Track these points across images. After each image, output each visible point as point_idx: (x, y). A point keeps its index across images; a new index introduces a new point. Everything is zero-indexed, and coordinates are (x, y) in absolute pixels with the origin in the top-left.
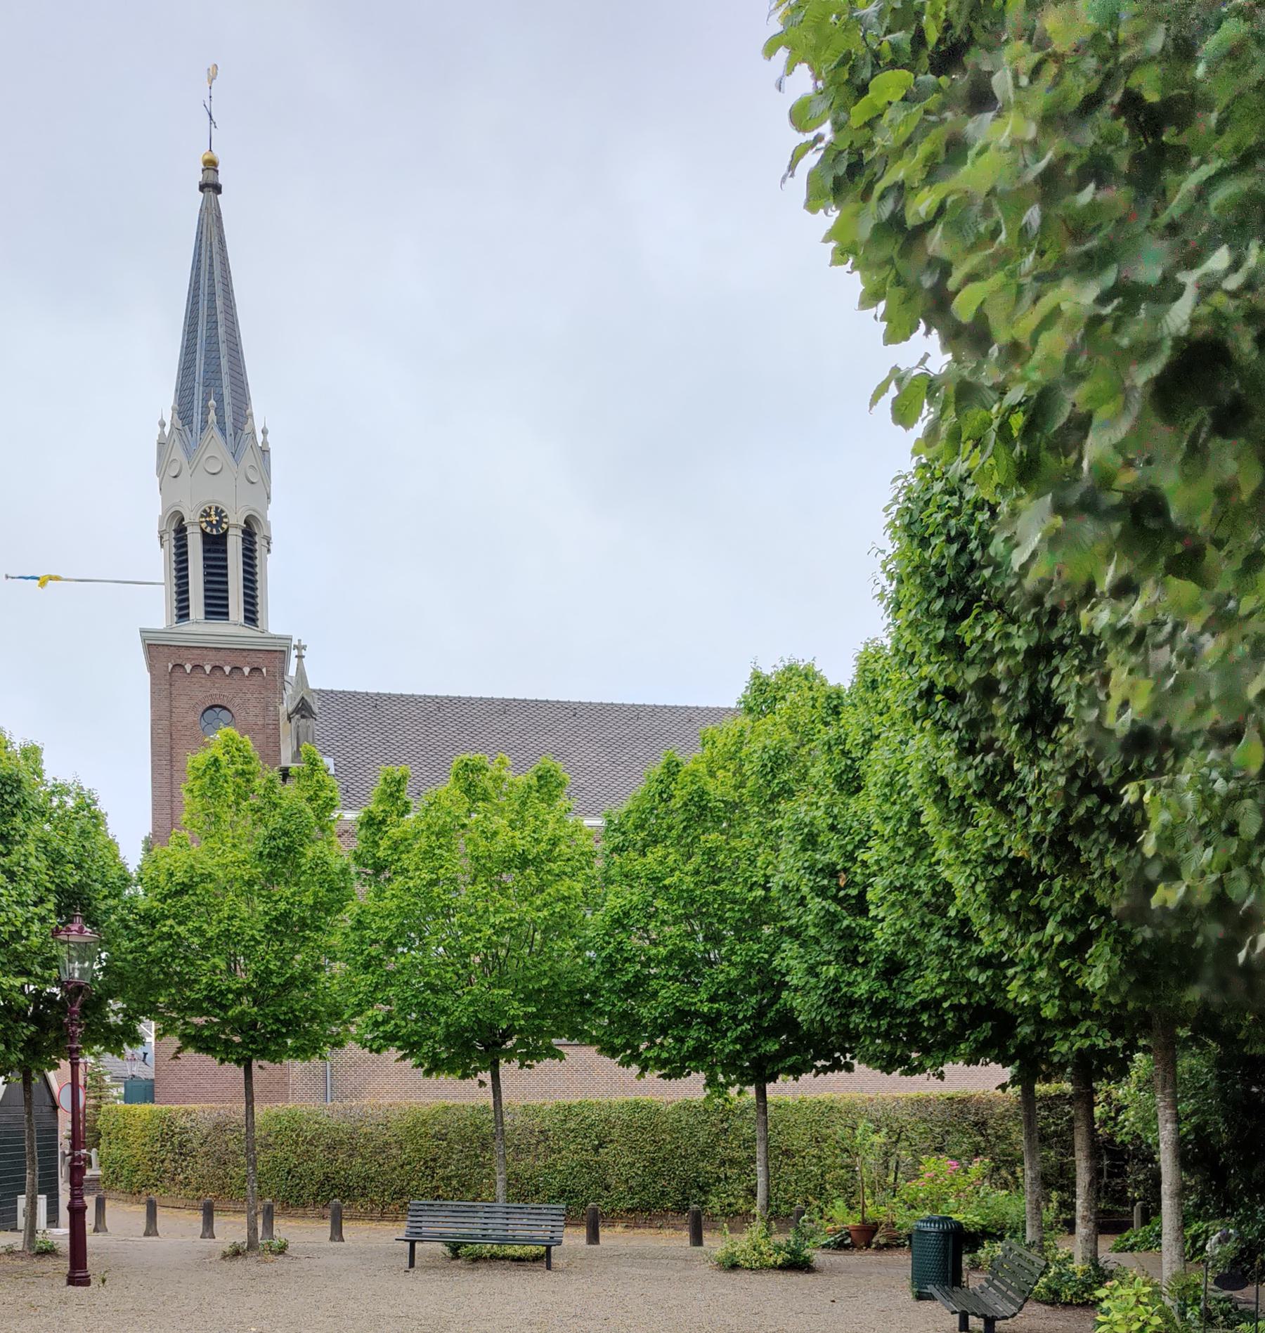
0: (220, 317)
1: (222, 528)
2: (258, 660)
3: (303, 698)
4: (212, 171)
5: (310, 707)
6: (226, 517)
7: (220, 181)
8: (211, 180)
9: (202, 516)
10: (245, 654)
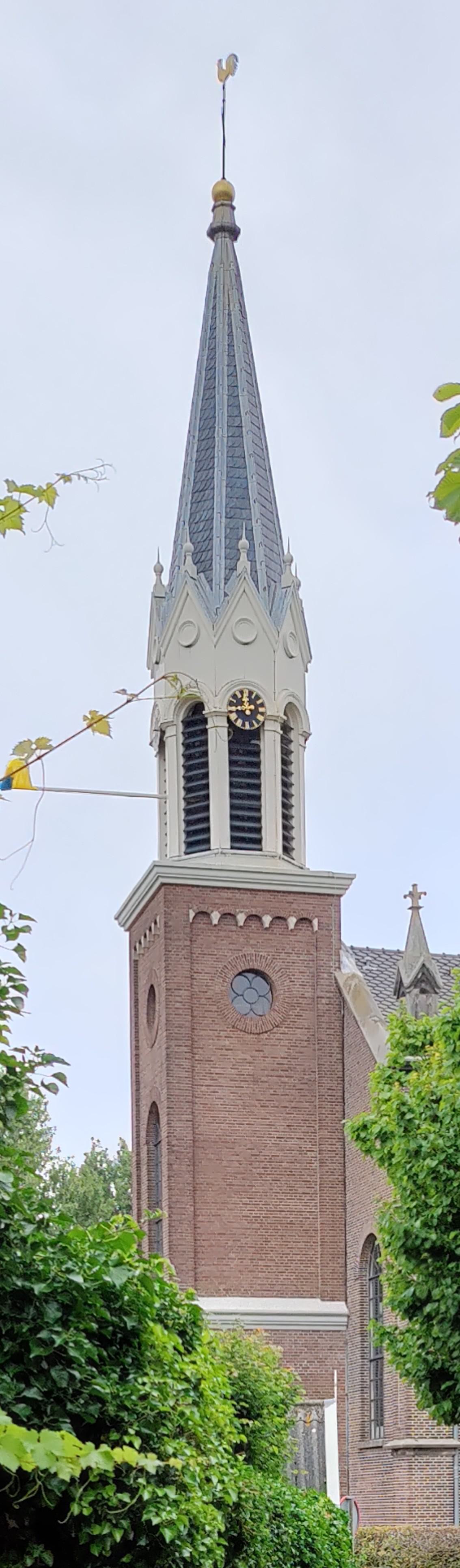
0: (245, 419)
1: (258, 722)
2: (305, 907)
3: (424, 965)
4: (228, 209)
5: (434, 978)
6: (262, 705)
7: (238, 224)
8: (226, 222)
9: (231, 704)
10: (290, 898)
